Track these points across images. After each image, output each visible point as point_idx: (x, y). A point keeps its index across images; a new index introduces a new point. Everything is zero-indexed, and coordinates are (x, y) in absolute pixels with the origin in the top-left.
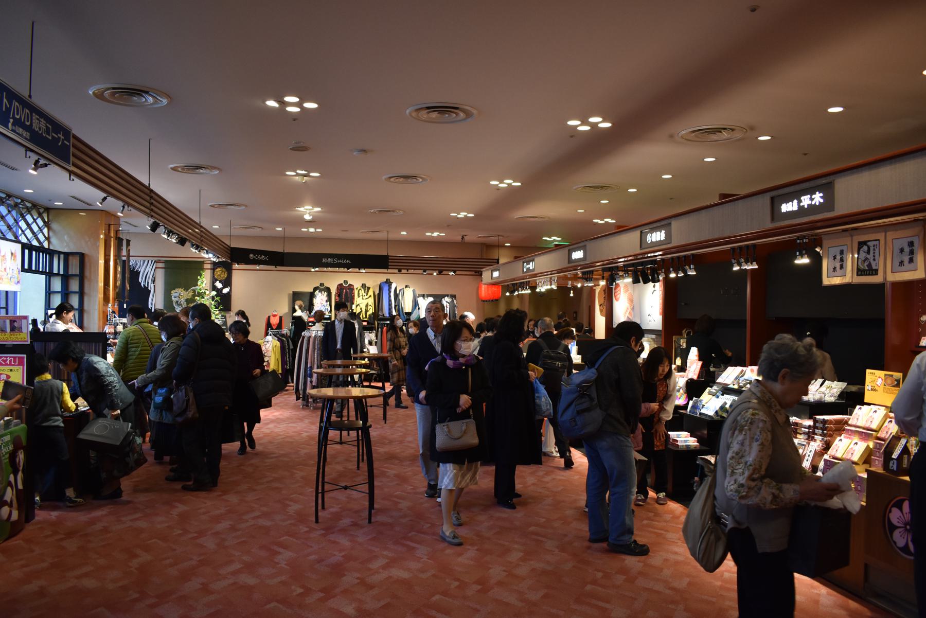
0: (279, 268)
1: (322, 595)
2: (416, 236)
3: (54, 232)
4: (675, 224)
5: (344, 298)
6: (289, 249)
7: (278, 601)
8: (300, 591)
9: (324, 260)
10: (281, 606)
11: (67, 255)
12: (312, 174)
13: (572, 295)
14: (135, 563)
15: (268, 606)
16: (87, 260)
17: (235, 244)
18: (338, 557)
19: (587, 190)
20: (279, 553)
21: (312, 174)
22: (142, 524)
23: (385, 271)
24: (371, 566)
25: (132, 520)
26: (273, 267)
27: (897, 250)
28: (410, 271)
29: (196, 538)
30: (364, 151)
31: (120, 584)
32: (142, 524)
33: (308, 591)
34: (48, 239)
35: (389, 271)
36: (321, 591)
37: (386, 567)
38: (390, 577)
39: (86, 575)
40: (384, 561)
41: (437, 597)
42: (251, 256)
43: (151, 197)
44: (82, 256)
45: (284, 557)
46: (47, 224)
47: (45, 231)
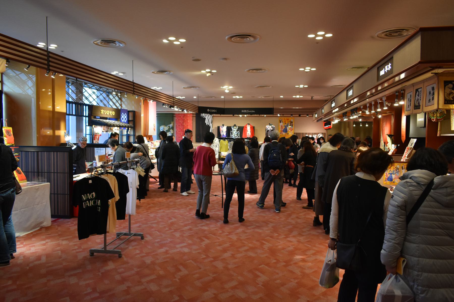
0: (222, 115)
1: (212, 259)
2: (288, 97)
3: (124, 102)
4: (355, 85)
5: (241, 130)
6: (226, 107)
7: (193, 260)
8: (275, 261)
9: (208, 110)
10: (266, 267)
11: (129, 112)
12: (213, 71)
13: (361, 126)
14: (203, 244)
15: (261, 266)
16: (136, 114)
17: (200, 105)
18: (291, 248)
19: (354, 69)
20: (265, 244)
21: (213, 71)
22: (205, 228)
23: (272, 115)
24: (307, 253)
25: (201, 226)
26: (219, 115)
27: (428, 93)
28: (284, 115)
29: (227, 235)
30: (225, 59)
31: (198, 251)
32: (205, 228)
33: (278, 261)
34: (121, 105)
35: (274, 115)
36: (213, 258)
37: (314, 254)
38: (317, 259)
39: (185, 246)
40: (314, 252)
41: (262, 266)
42: (208, 110)
43: (134, 86)
44: (134, 112)
45: (267, 245)
46: (120, 99)
47: (119, 102)
